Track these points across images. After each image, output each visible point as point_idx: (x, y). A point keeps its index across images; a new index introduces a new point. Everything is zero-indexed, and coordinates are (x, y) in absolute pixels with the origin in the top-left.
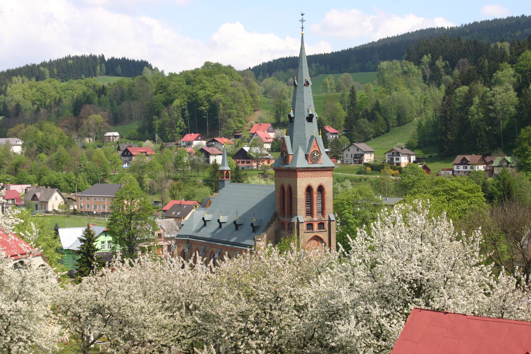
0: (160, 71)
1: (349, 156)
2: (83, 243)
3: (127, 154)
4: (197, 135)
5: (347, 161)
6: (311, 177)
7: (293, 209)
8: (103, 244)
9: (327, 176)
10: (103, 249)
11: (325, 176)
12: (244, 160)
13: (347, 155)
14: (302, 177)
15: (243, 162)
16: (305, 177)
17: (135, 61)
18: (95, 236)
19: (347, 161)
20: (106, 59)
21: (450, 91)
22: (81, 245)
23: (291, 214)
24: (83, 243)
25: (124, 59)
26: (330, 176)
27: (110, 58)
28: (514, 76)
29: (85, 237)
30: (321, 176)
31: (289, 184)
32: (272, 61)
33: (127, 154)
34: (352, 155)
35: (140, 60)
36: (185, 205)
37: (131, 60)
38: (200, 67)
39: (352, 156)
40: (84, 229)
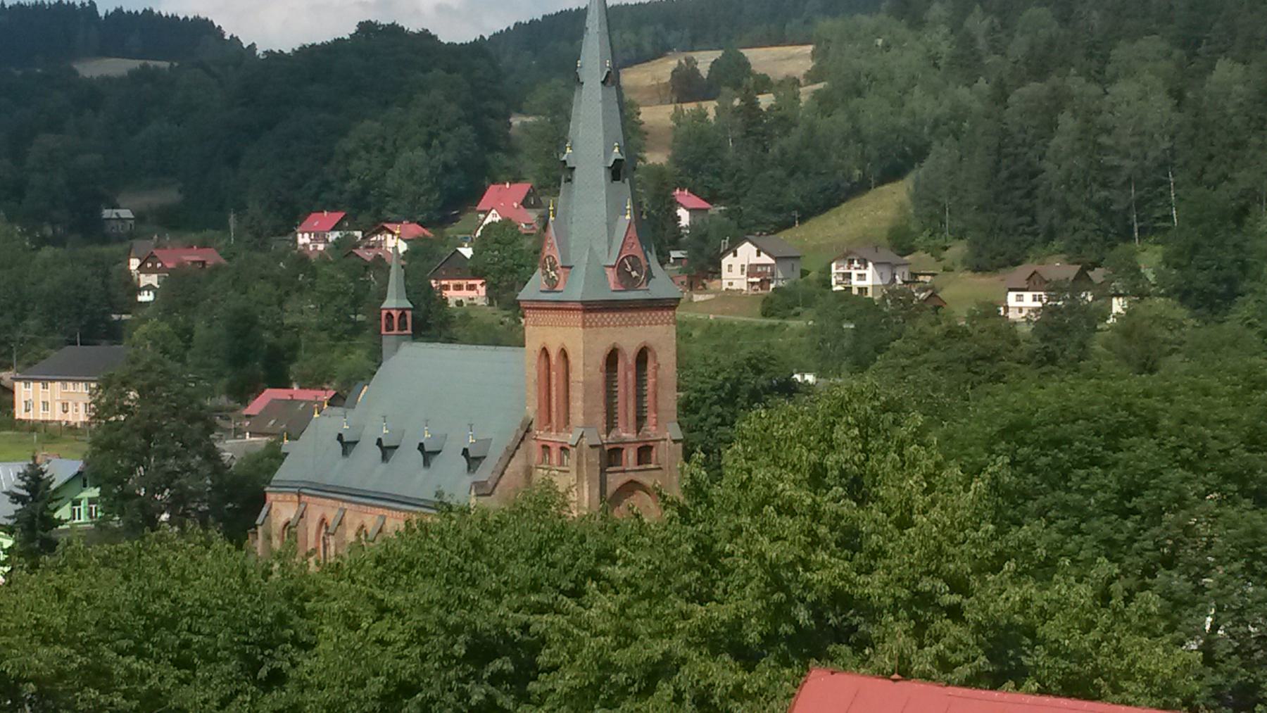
0: (245, 46)
1: (737, 269)
2: (19, 506)
3: (154, 265)
4: (340, 215)
5: (731, 284)
6: (620, 325)
7: (571, 411)
8: (77, 508)
9: (662, 323)
10: (77, 521)
11: (656, 324)
12: (461, 282)
13: (730, 266)
14: (597, 326)
15: (458, 288)
16: (603, 326)
17: (177, 18)
18: (53, 487)
19: (731, 284)
20: (102, 14)
21: (1000, 96)
22: (16, 511)
23: (568, 423)
24: (19, 506)
25: (148, 13)
26: (668, 323)
27: (111, 10)
28: (1168, 56)
29: (23, 488)
30: (644, 324)
31: (563, 344)
32: (540, 19)
33: (154, 265)
34: (743, 266)
35: (191, 17)
36: (302, 401)
37: (167, 16)
38: (347, 37)
39: (743, 270)
40: (20, 467)
